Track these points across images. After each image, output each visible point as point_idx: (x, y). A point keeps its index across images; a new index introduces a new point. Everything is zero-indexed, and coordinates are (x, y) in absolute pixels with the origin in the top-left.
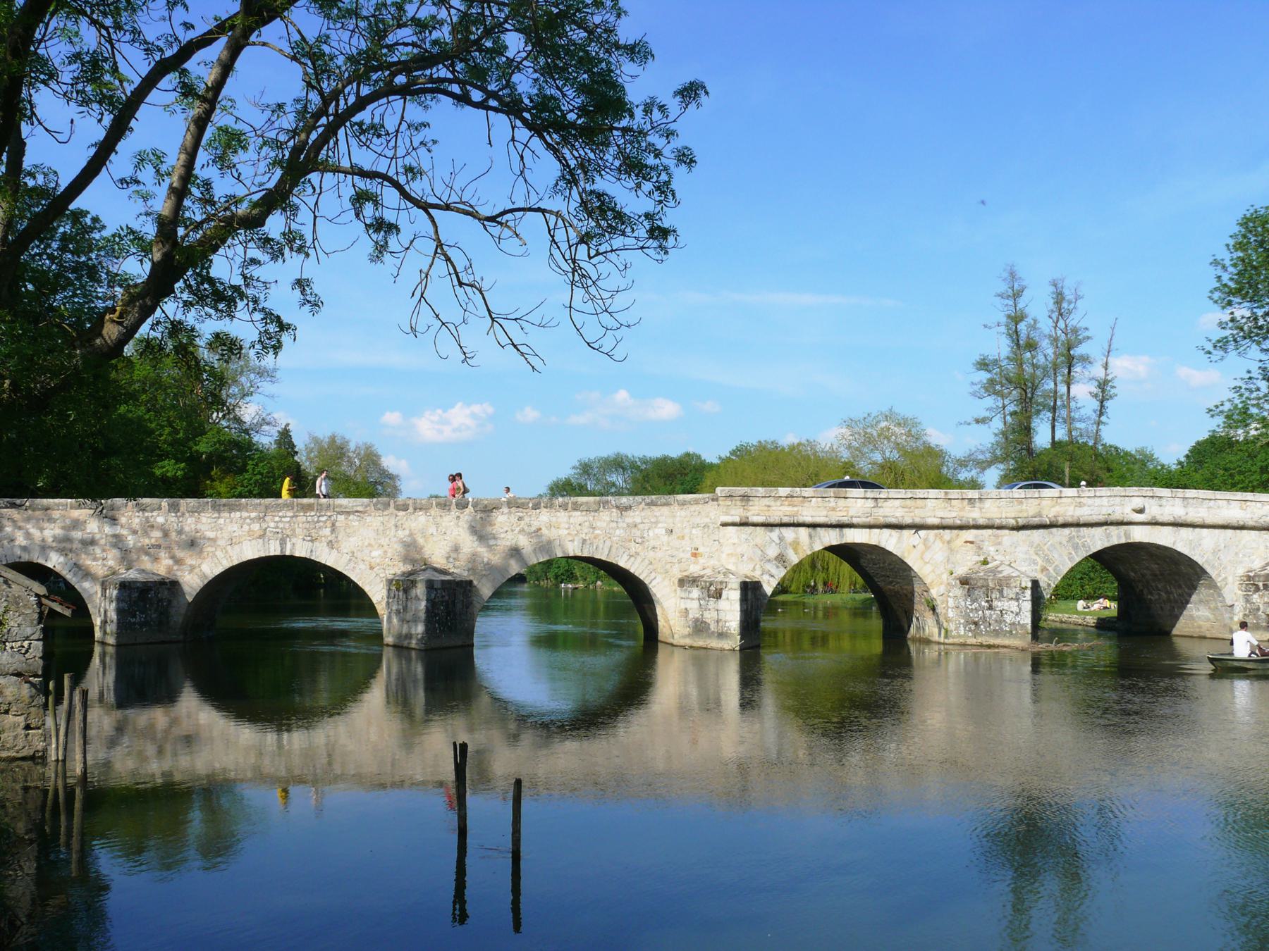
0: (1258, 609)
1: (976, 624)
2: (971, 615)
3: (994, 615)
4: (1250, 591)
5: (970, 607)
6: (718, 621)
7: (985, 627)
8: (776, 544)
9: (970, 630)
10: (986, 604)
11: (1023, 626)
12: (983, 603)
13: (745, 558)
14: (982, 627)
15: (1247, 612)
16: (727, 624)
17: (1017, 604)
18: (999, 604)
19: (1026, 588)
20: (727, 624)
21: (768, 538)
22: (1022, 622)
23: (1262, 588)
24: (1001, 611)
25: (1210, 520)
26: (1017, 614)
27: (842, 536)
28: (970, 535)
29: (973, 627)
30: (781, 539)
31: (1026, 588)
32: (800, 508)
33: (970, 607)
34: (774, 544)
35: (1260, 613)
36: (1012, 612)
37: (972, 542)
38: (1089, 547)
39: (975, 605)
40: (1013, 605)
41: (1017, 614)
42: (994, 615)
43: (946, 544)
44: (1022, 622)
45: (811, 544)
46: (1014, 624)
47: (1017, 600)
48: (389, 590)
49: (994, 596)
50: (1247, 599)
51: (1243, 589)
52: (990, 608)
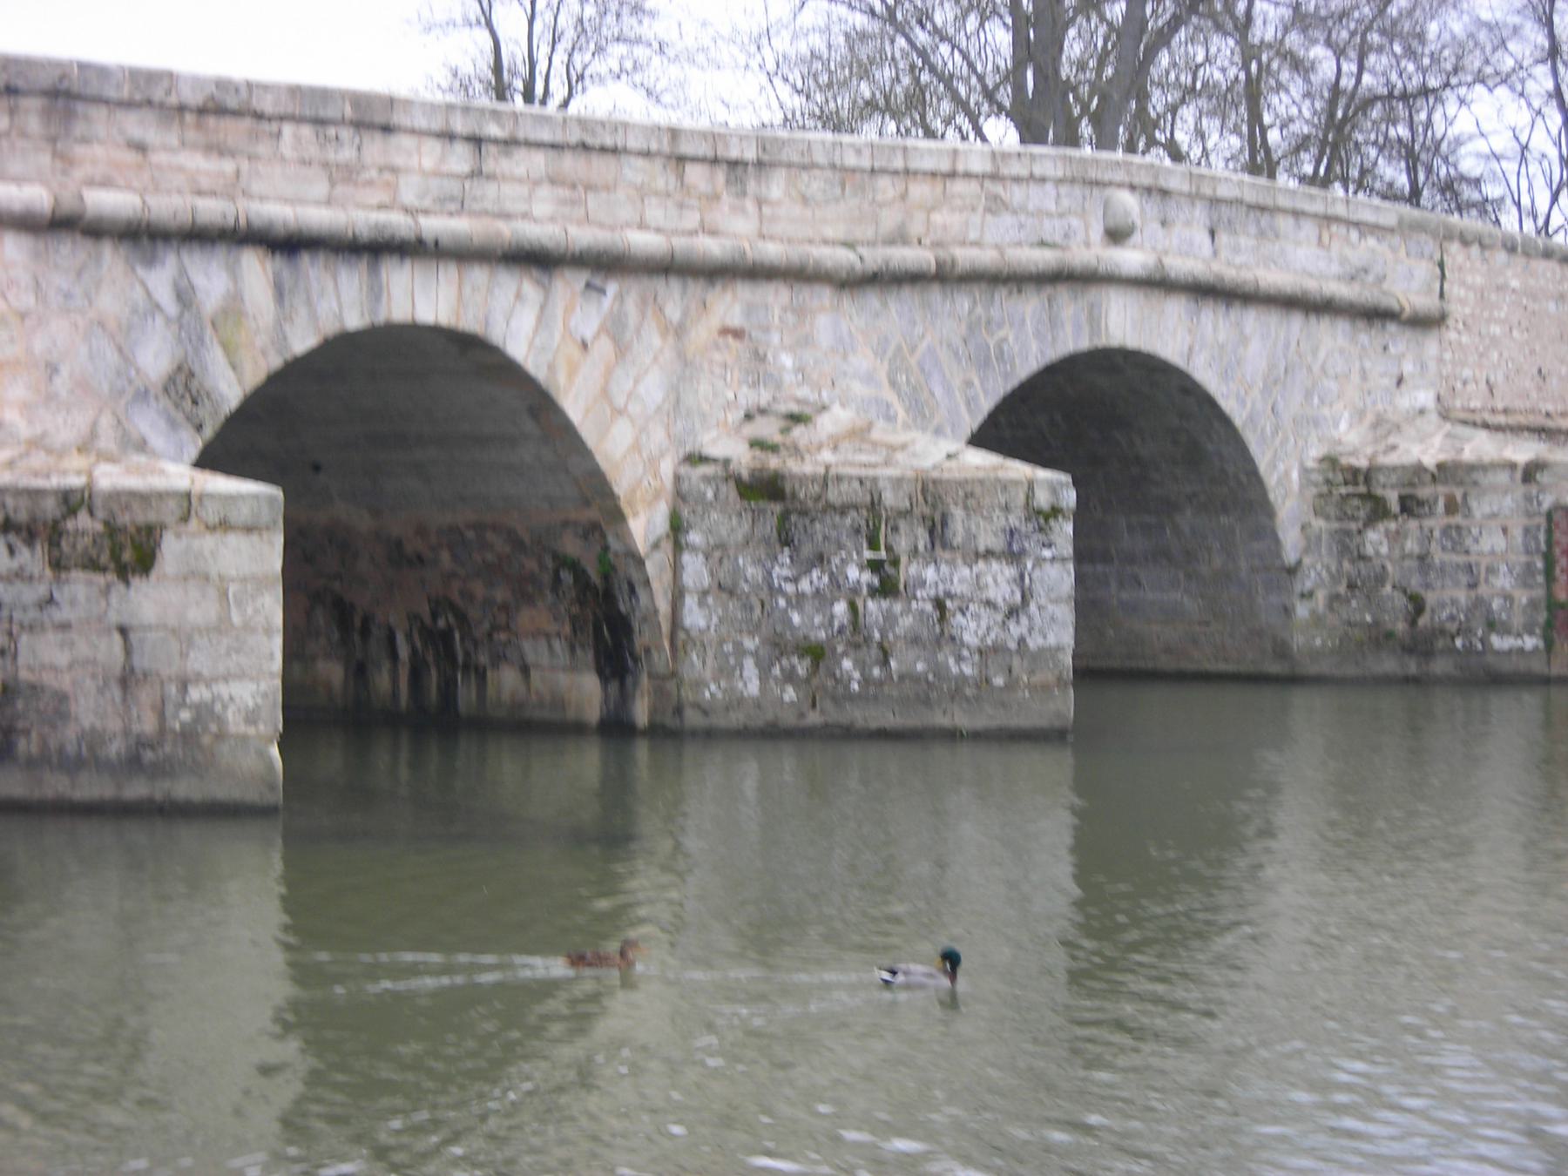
0: (1381, 578)
1: (817, 654)
2: (796, 618)
3: (906, 618)
4: (1354, 518)
5: (789, 588)
6: (128, 679)
7: (861, 665)
8: (168, 320)
9: (790, 677)
10: (867, 577)
11: (1048, 654)
12: (853, 573)
13: (62, 383)
14: (847, 664)
15: (1342, 589)
16: (196, 694)
17: (1010, 572)
18: (930, 574)
19: (1055, 511)
20: (196, 694)
21: (138, 294)
22: (1034, 643)
23: (1395, 506)
24: (939, 604)
25: (1273, 278)
26: (1013, 612)
27: (376, 293)
28: (730, 305)
29: (802, 668)
30: (185, 296)
31: (1055, 511)
32: (245, 166)
33: (789, 588)
34: (159, 320)
35: (1388, 588)
36: (989, 604)
37: (738, 334)
38: (1013, 366)
39: (816, 579)
40: (999, 581)
41: (1013, 612)
42: (906, 618)
43: (671, 339)
44: (1034, 643)
45: (279, 325)
46: (998, 649)
47: (1013, 556)
48: (138, 371)
49: (902, 544)
50: (1347, 546)
51: (1332, 511)
52: (887, 588)
